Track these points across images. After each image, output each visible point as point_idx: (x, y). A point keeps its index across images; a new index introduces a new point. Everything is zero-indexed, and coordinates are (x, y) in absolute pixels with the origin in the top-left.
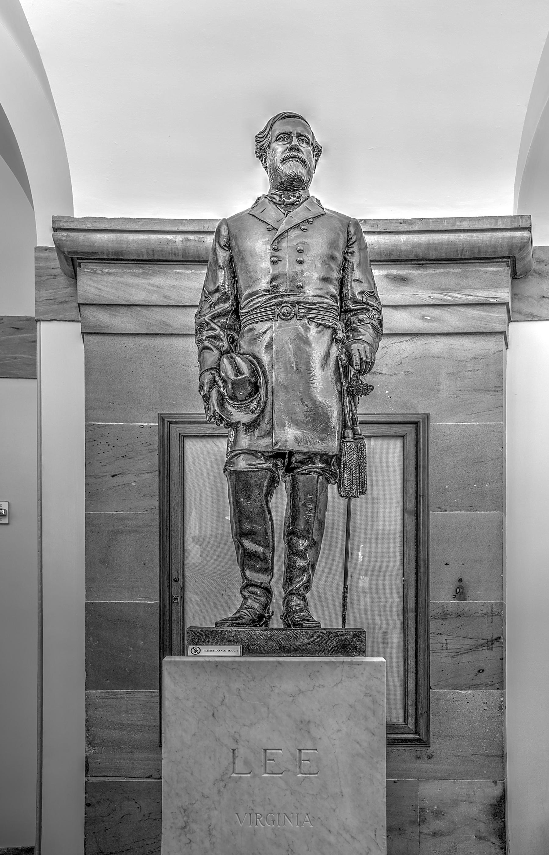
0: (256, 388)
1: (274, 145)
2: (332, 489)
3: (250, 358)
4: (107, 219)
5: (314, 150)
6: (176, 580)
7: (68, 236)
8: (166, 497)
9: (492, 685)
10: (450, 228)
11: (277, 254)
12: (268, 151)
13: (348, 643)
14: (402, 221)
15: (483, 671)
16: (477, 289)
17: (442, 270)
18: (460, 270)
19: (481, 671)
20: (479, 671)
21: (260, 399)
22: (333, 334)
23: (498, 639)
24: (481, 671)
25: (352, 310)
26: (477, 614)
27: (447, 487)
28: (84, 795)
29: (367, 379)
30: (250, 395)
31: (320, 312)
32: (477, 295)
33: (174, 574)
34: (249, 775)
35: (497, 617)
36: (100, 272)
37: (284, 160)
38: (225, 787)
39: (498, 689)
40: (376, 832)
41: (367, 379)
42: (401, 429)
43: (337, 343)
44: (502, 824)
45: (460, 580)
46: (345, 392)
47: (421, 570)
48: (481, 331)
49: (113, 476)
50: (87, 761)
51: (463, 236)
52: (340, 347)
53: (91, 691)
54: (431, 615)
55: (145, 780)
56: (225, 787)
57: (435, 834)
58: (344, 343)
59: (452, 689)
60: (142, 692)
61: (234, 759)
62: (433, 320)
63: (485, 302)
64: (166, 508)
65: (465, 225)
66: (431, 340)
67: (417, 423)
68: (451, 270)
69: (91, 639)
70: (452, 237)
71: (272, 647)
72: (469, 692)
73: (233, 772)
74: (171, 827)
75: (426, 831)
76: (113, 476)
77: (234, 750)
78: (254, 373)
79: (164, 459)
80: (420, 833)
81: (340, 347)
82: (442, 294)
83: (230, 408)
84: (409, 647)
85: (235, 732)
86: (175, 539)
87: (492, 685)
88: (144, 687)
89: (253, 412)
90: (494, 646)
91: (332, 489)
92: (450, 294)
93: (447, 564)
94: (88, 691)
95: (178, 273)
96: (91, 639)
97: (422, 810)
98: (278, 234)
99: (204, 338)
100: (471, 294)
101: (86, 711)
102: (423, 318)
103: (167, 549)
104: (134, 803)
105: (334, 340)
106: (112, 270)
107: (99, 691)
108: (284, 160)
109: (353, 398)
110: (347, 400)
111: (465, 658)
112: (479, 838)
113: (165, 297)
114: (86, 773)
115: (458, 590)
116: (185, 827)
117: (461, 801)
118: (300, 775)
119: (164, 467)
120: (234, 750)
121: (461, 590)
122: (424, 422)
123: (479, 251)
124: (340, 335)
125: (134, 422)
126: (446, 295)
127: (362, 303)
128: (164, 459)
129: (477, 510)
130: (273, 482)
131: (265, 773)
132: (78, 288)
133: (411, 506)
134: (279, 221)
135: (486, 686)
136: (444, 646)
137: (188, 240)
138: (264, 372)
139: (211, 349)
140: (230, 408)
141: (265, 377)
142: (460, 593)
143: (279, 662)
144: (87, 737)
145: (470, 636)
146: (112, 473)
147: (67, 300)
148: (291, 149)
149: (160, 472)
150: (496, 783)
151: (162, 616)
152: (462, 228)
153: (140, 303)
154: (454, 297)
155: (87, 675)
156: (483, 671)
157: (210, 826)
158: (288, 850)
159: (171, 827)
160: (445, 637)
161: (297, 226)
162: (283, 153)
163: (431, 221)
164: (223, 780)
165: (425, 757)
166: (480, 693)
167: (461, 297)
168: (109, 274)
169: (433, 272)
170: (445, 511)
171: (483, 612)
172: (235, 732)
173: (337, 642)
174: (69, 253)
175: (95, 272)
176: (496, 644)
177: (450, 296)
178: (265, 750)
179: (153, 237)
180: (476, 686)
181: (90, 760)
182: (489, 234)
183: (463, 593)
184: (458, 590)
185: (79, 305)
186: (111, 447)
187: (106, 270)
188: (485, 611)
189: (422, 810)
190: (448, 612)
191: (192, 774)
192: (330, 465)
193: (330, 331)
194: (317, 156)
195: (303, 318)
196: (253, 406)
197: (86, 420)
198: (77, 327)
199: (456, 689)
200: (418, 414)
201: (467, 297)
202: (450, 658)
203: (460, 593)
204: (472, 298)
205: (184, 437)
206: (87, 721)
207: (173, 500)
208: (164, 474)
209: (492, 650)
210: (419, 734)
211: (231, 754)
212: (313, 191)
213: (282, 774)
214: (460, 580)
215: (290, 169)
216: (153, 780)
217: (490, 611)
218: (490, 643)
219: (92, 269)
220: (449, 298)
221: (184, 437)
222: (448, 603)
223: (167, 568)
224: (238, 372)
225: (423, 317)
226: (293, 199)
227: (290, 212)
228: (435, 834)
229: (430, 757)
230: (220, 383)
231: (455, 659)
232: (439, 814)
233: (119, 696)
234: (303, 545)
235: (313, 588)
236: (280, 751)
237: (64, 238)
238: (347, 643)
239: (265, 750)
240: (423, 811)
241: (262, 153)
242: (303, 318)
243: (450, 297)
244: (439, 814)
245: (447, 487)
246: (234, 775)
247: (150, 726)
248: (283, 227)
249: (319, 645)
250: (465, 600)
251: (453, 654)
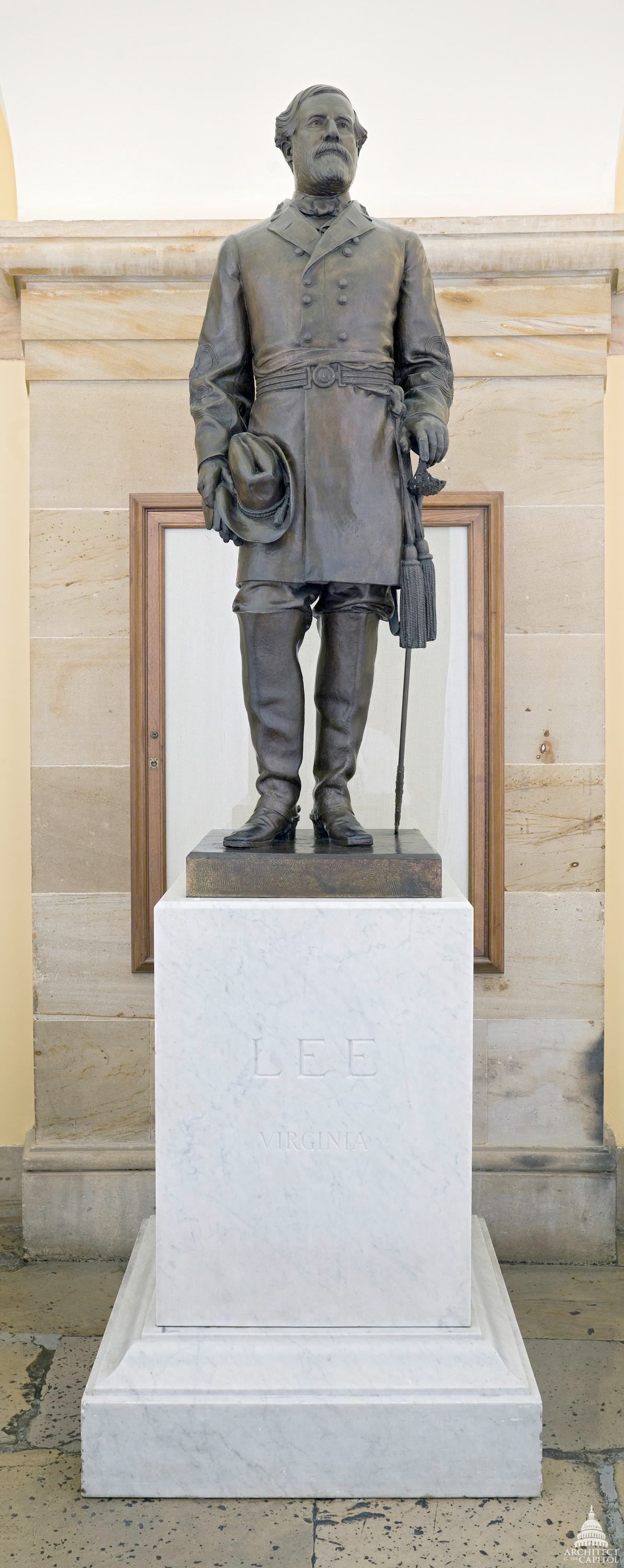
0: (282, 488)
1: (304, 132)
2: (383, 626)
3: (272, 441)
4: (62, 222)
5: (357, 137)
6: (155, 736)
7: (9, 248)
8: (141, 617)
9: (590, 884)
10: (531, 231)
11: (311, 290)
12: (293, 140)
13: (415, 877)
14: (464, 220)
15: (578, 864)
16: (567, 314)
17: (519, 288)
18: (543, 288)
19: (575, 865)
20: (572, 865)
21: (288, 507)
22: (387, 405)
23: (599, 818)
24: (575, 865)
25: (412, 364)
26: (569, 783)
27: (527, 598)
28: (32, 1040)
29: (434, 472)
30: (272, 502)
31: (371, 375)
32: (568, 322)
33: (152, 728)
34: (277, 1077)
35: (597, 786)
36: (51, 295)
37: (319, 154)
38: (243, 1094)
39: (598, 890)
40: (456, 1157)
41: (434, 472)
42: (466, 516)
43: (394, 418)
44: (599, 1079)
45: (547, 734)
46: (406, 491)
47: (493, 721)
48: (573, 374)
49: (68, 585)
50: (35, 993)
51: (549, 241)
52: (398, 425)
53: (39, 894)
54: (506, 783)
55: (113, 1020)
56: (243, 1094)
57: (508, 1095)
58: (403, 418)
59: (535, 890)
60: (108, 896)
61: (256, 1053)
62: (507, 357)
63: (578, 333)
64: (141, 632)
65: (552, 226)
66: (505, 385)
67: (486, 507)
68: (531, 287)
69: (38, 819)
70: (535, 243)
71: (309, 883)
72: (558, 894)
73: (256, 1073)
74: (169, 1151)
75: (496, 1090)
76: (68, 585)
77: (256, 1041)
78: (280, 466)
79: (137, 561)
80: (489, 1093)
81: (398, 425)
82: (519, 321)
83: (243, 518)
84: (477, 831)
85: (258, 1014)
86: (153, 677)
87: (590, 884)
88: (111, 888)
89: (278, 526)
90: (592, 828)
91: (383, 626)
92: (530, 321)
93: (528, 710)
94: (35, 894)
95: (158, 294)
96: (38, 819)
97: (492, 1062)
98: (311, 262)
99: (204, 408)
100: (559, 321)
101: (33, 923)
102: (493, 354)
103: (141, 691)
104: (99, 1051)
105: (390, 413)
106: (68, 293)
107: (51, 894)
108: (319, 154)
109: (417, 499)
110: (408, 499)
111: (553, 846)
112: (568, 1098)
113: (139, 327)
114: (35, 1010)
115: (543, 748)
116: (189, 1151)
117: (544, 1048)
118: (350, 1077)
119: (138, 572)
120: (256, 1041)
121: (548, 748)
122: (496, 506)
123: (571, 263)
124: (399, 407)
125: (96, 506)
126: (524, 323)
127: (425, 354)
128: (137, 561)
129: (569, 632)
130: (304, 625)
131: (301, 1073)
132: (22, 317)
133: (479, 628)
134: (313, 243)
135: (582, 885)
136: (525, 829)
137: (171, 249)
138: (292, 465)
139: (214, 426)
140: (243, 518)
141: (294, 472)
142: (546, 752)
143: (321, 911)
144: (34, 959)
145: (560, 814)
146: (67, 582)
147: (5, 330)
148: (328, 138)
149: (131, 579)
150: (592, 1023)
151: (135, 785)
152: (547, 230)
153: (105, 337)
154: (535, 325)
155: (33, 871)
156: (578, 864)
157: (223, 1150)
158: (333, 1185)
159: (169, 1151)
160: (526, 816)
161: (339, 249)
162: (316, 143)
163: (505, 219)
164: (240, 1084)
165: (497, 987)
166: (573, 896)
167: (546, 326)
168: (64, 297)
169: (506, 290)
170: (526, 632)
171: (578, 780)
172: (258, 1014)
173: (401, 875)
174: (11, 270)
175: (44, 295)
176: (596, 826)
177: (530, 324)
178: (301, 1040)
179: (125, 246)
180: (568, 886)
181: (39, 991)
182: (585, 239)
183: (550, 752)
184: (543, 748)
185: (23, 342)
186: (65, 542)
187: (60, 293)
188: (580, 779)
189: (492, 1062)
190: (530, 780)
191: (197, 1075)
192: (384, 596)
193: (383, 402)
194: (360, 143)
195: (347, 384)
196: (278, 517)
197: (32, 505)
198: (19, 369)
199: (540, 890)
200: (488, 493)
201: (554, 325)
202: (532, 846)
203: (546, 752)
204: (560, 326)
205: (165, 528)
206: (34, 936)
207: (150, 620)
208: (137, 583)
209: (590, 834)
210: (489, 958)
211: (253, 1046)
212: (355, 193)
213: (324, 1075)
214: (547, 734)
215: (326, 167)
216: (125, 1020)
217: (587, 778)
218: (587, 825)
219: (41, 291)
220: (529, 327)
221: (164, 527)
222: (530, 767)
223: (141, 719)
224: (257, 468)
225: (494, 354)
226: (329, 208)
227: (327, 227)
228: (508, 1095)
229: (503, 988)
230: (228, 478)
231: (539, 847)
232: (514, 1067)
233: (77, 901)
234: (344, 714)
235: (354, 777)
236: (322, 1042)
237: (5, 251)
238: (416, 877)
239: (301, 1040)
240: (492, 1063)
241: (284, 142)
242: (347, 384)
243: (531, 325)
244: (514, 1067)
245: (527, 598)
246: (256, 1077)
247: (119, 944)
248: (318, 252)
249: (376, 881)
250: (552, 761)
251: (537, 840)
